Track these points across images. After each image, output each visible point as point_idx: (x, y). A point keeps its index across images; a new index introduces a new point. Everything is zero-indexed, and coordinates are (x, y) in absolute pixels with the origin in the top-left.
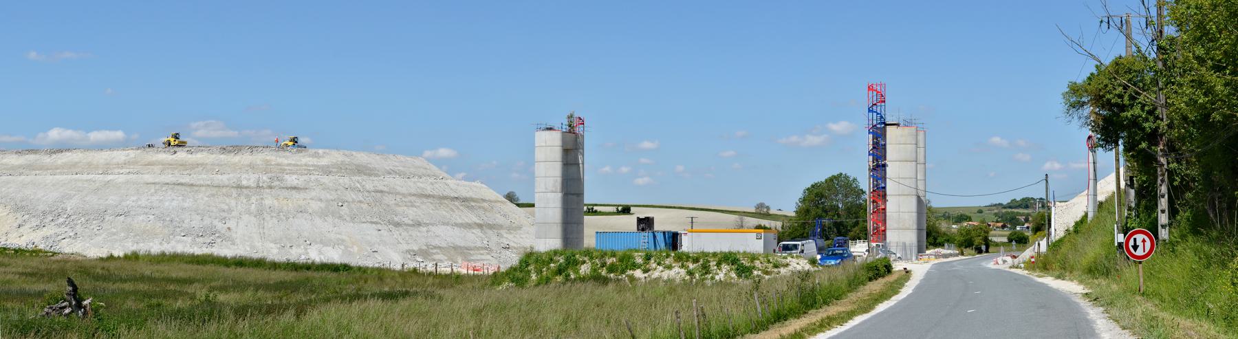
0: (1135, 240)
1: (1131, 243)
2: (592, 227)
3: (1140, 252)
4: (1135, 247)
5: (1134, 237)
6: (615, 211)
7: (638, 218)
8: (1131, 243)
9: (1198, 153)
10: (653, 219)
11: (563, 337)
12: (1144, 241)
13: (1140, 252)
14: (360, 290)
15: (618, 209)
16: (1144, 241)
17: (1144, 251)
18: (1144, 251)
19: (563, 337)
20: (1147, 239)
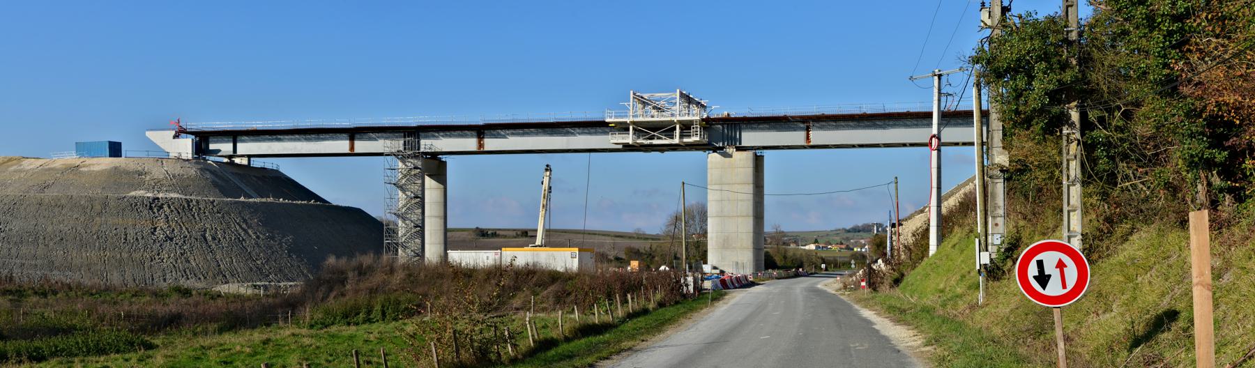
0: (1040, 263)
1: (1033, 270)
2: (419, 182)
3: (1054, 289)
4: (1043, 279)
5: (1038, 257)
6: (515, 235)
7: (1060, 260)
8: (1033, 270)
9: (242, 208)
10: (121, 143)
11: (408, 367)
12: (1061, 265)
13: (1054, 289)
14: (167, 296)
15: (517, 234)
16: (1061, 265)
17: (1064, 287)
18: (1064, 287)
19: (408, 367)
20: (1067, 260)
